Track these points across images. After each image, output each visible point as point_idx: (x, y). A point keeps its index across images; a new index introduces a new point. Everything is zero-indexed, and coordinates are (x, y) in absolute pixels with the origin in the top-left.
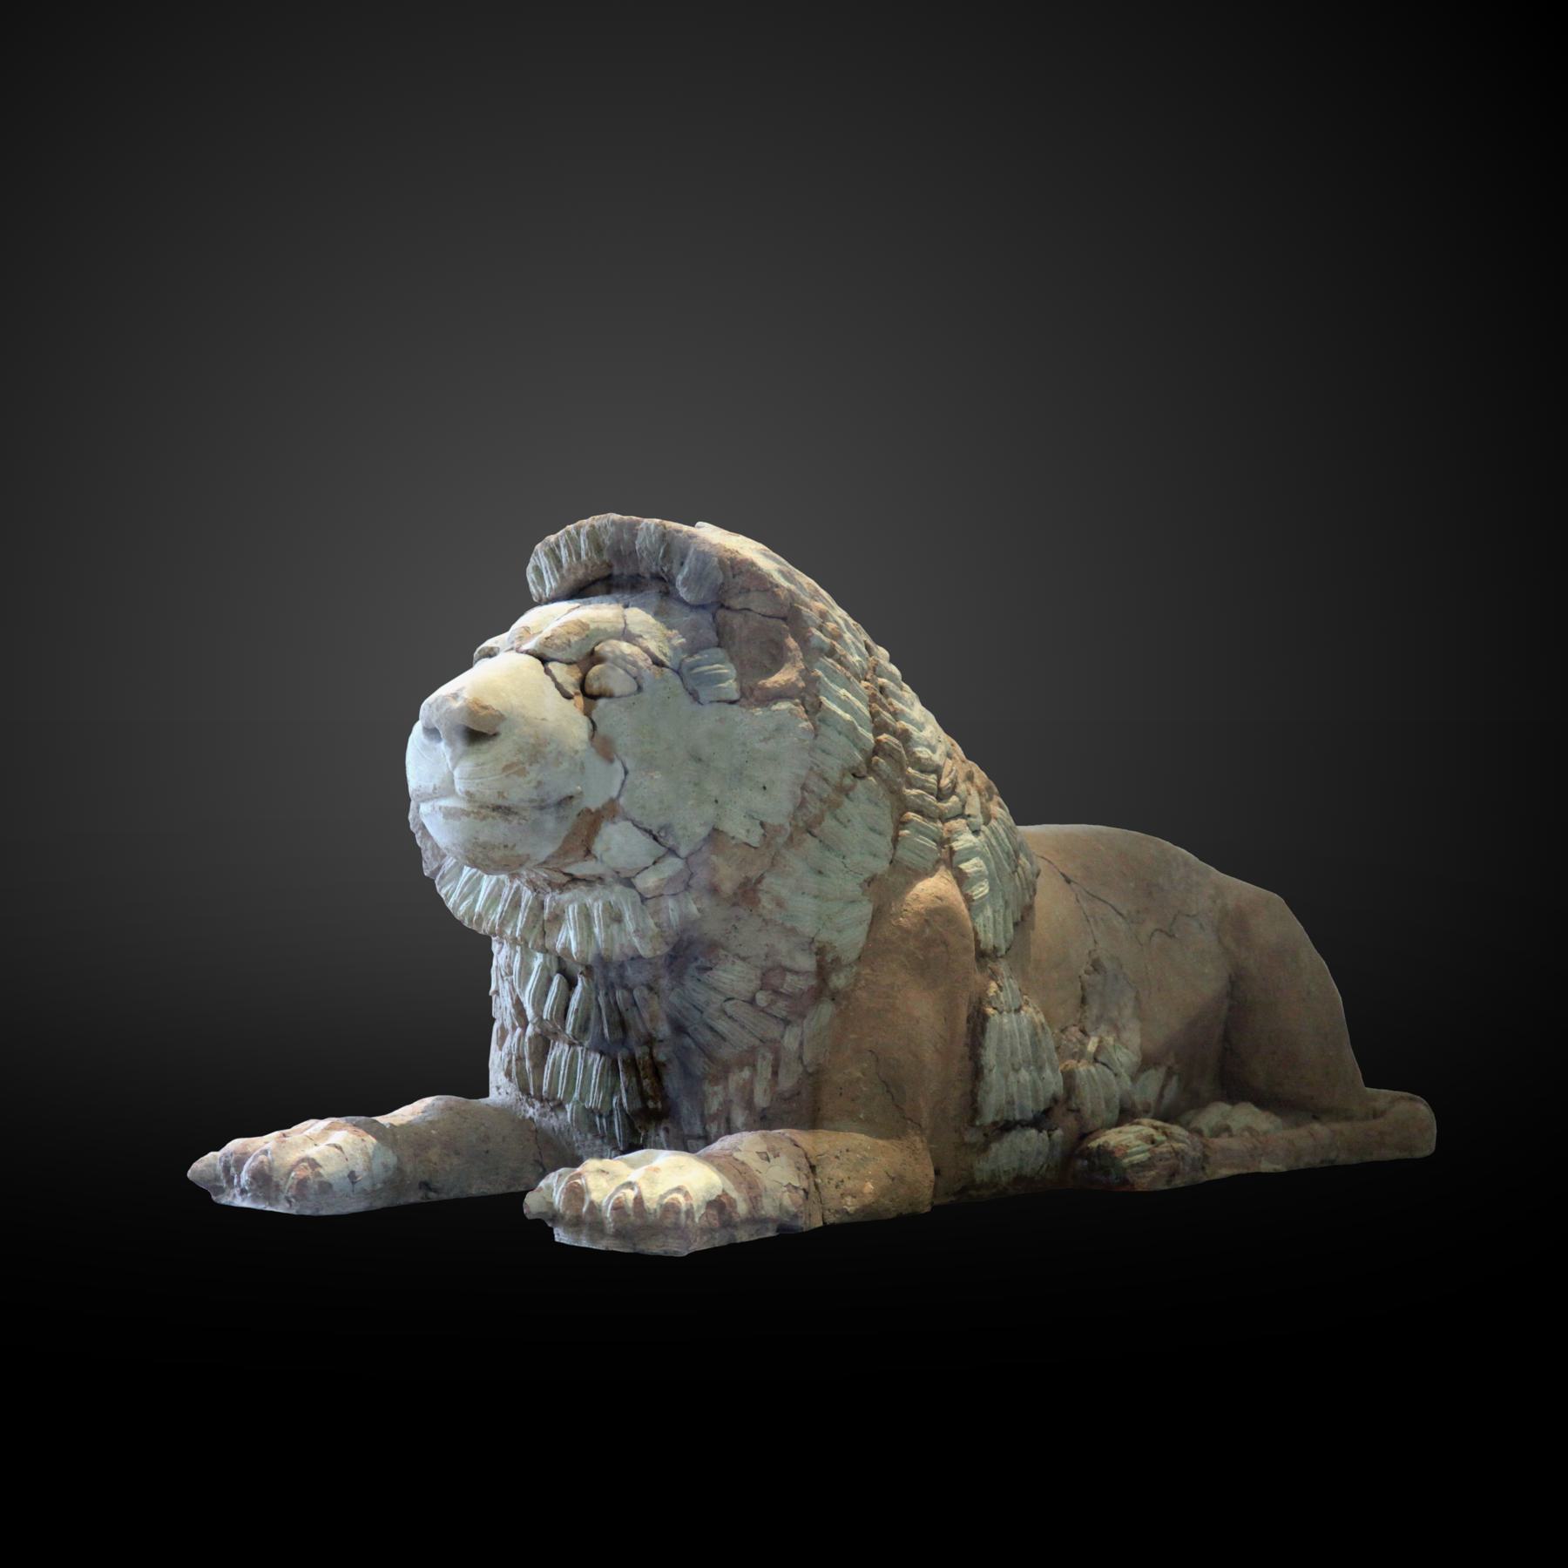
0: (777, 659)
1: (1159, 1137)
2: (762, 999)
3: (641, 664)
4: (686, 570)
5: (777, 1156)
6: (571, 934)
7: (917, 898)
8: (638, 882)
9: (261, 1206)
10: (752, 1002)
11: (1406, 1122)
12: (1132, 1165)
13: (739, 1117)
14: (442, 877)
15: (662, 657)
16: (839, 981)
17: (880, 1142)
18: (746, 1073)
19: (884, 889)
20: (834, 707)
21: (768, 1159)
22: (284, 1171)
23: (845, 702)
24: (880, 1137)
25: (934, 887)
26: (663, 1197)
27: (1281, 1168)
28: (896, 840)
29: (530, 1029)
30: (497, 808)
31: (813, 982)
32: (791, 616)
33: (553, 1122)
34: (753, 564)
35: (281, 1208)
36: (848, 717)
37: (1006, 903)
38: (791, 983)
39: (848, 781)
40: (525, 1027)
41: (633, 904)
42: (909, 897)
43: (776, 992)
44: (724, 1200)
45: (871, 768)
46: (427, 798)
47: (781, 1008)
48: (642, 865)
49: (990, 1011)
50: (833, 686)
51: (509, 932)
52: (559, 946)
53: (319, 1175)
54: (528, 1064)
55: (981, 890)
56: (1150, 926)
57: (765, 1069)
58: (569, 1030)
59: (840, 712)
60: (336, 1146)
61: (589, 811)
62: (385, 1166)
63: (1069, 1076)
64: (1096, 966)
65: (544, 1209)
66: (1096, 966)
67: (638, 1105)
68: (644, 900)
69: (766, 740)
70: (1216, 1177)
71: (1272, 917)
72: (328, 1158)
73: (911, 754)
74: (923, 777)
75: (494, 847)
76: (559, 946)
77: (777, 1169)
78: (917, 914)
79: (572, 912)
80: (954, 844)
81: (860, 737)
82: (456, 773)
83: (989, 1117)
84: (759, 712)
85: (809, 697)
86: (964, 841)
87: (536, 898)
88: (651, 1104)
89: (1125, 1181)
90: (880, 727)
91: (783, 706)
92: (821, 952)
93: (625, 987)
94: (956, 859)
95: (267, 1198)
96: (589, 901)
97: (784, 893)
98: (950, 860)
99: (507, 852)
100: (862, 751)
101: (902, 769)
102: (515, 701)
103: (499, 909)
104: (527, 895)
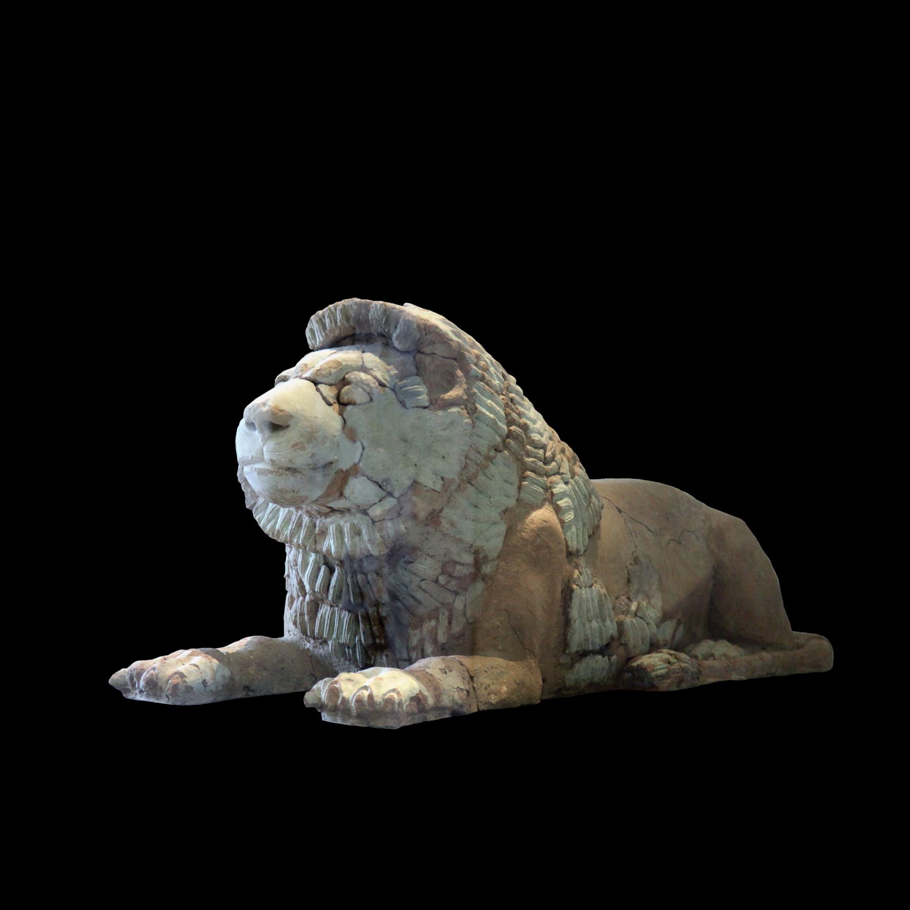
0: (451, 382)
1: (673, 660)
2: (442, 579)
3: (372, 385)
4: (398, 331)
5: (451, 671)
6: (332, 542)
7: (532, 521)
8: (370, 512)
9: (152, 700)
10: (436, 581)
11: (816, 651)
12: (657, 676)
13: (429, 648)
14: (257, 509)
15: (384, 382)
16: (487, 569)
17: (511, 663)
18: (433, 623)
19: (513, 516)
20: (484, 410)
21: (446, 673)
22: (165, 679)
23: (490, 408)
24: (511, 660)
25: (542, 515)
26: (385, 695)
27: (743, 678)
28: (520, 488)
29: (307, 597)
30: (288, 469)
31: (472, 570)
32: (459, 358)
33: (321, 651)
34: (437, 327)
35: (163, 701)
36: (492, 416)
37: (584, 524)
38: (459, 571)
39: (492, 453)
40: (304, 596)
41: (368, 525)
42: (528, 521)
43: (450, 576)
44: (420, 696)
45: (506, 446)
46: (248, 463)
47: (453, 585)
48: (373, 502)
49: (575, 587)
50: (483, 398)
51: (295, 541)
52: (324, 549)
53: (185, 682)
54: (306, 617)
55: (569, 517)
56: (668, 537)
57: (444, 620)
58: (330, 598)
59: (487, 413)
60: (195, 665)
61: (342, 470)
62: (224, 677)
63: (620, 625)
64: (636, 561)
65: (316, 702)
66: (636, 561)
67: (370, 641)
68: (374, 522)
69: (444, 429)
70: (706, 683)
71: (737, 531)
72: (190, 672)
73: (528, 437)
74: (536, 451)
75: (286, 492)
76: (324, 549)
77: (451, 678)
78: (532, 530)
79: (332, 529)
80: (554, 490)
81: (499, 428)
82: (265, 449)
83: (574, 648)
84: (440, 413)
85: (469, 405)
86: (560, 488)
87: (311, 521)
88: (378, 641)
89: (653, 686)
90: (511, 422)
91: (454, 410)
92: (476, 552)
93: (363, 573)
94: (555, 498)
95: (155, 695)
96: (342, 523)
97: (455, 518)
98: (551, 499)
99: (294, 495)
100: (500, 436)
101: (524, 447)
102: (299, 407)
103: (290, 528)
104: (306, 519)
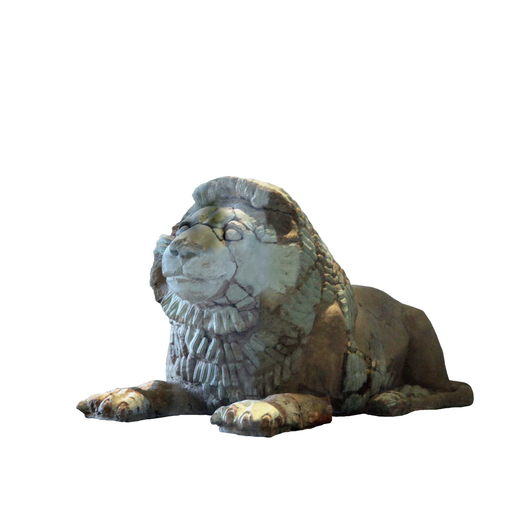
0: (289, 228)
1: (398, 397)
2: (279, 347)
3: (243, 229)
4: (255, 196)
5: (289, 403)
6: (214, 323)
7: (330, 312)
8: (238, 306)
10: (275, 348)
12: (391, 407)
13: (268, 389)
15: (249, 227)
16: (304, 341)
17: (318, 398)
18: (271, 373)
20: (306, 245)
21: (286, 404)
22: (116, 406)
25: (334, 308)
26: (262, 417)
28: (322, 292)
29: (189, 357)
30: (198, 279)
31: (296, 341)
33: (196, 390)
34: (280, 195)
37: (352, 314)
38: (290, 342)
39: (310, 271)
40: (186, 356)
41: (235, 313)
42: (327, 312)
43: (283, 345)
45: (316, 267)
46: (170, 275)
47: (285, 351)
48: (239, 300)
50: (306, 238)
51: (190, 322)
52: (209, 328)
53: (128, 408)
54: (187, 369)
55: (346, 310)
56: (384, 322)
57: (278, 371)
58: (207, 357)
59: (308, 247)
60: (132, 398)
62: (147, 405)
64: (372, 335)
66: (372, 335)
67: (229, 384)
68: (239, 312)
69: (287, 256)
72: (131, 402)
73: (326, 261)
74: (329, 269)
75: (196, 293)
76: (209, 328)
77: (290, 407)
78: (330, 318)
79: (214, 316)
80: (339, 293)
81: (313, 255)
82: (184, 267)
83: (346, 390)
84: (284, 246)
85: (298, 240)
86: (341, 292)
87: (201, 311)
88: (233, 384)
90: (318, 252)
91: (293, 245)
92: (300, 331)
93: (227, 342)
94: (339, 298)
96: (221, 312)
97: (289, 310)
98: (338, 299)
99: (201, 295)
100: (314, 260)
101: (323, 267)
103: (186, 314)
104: (197, 310)
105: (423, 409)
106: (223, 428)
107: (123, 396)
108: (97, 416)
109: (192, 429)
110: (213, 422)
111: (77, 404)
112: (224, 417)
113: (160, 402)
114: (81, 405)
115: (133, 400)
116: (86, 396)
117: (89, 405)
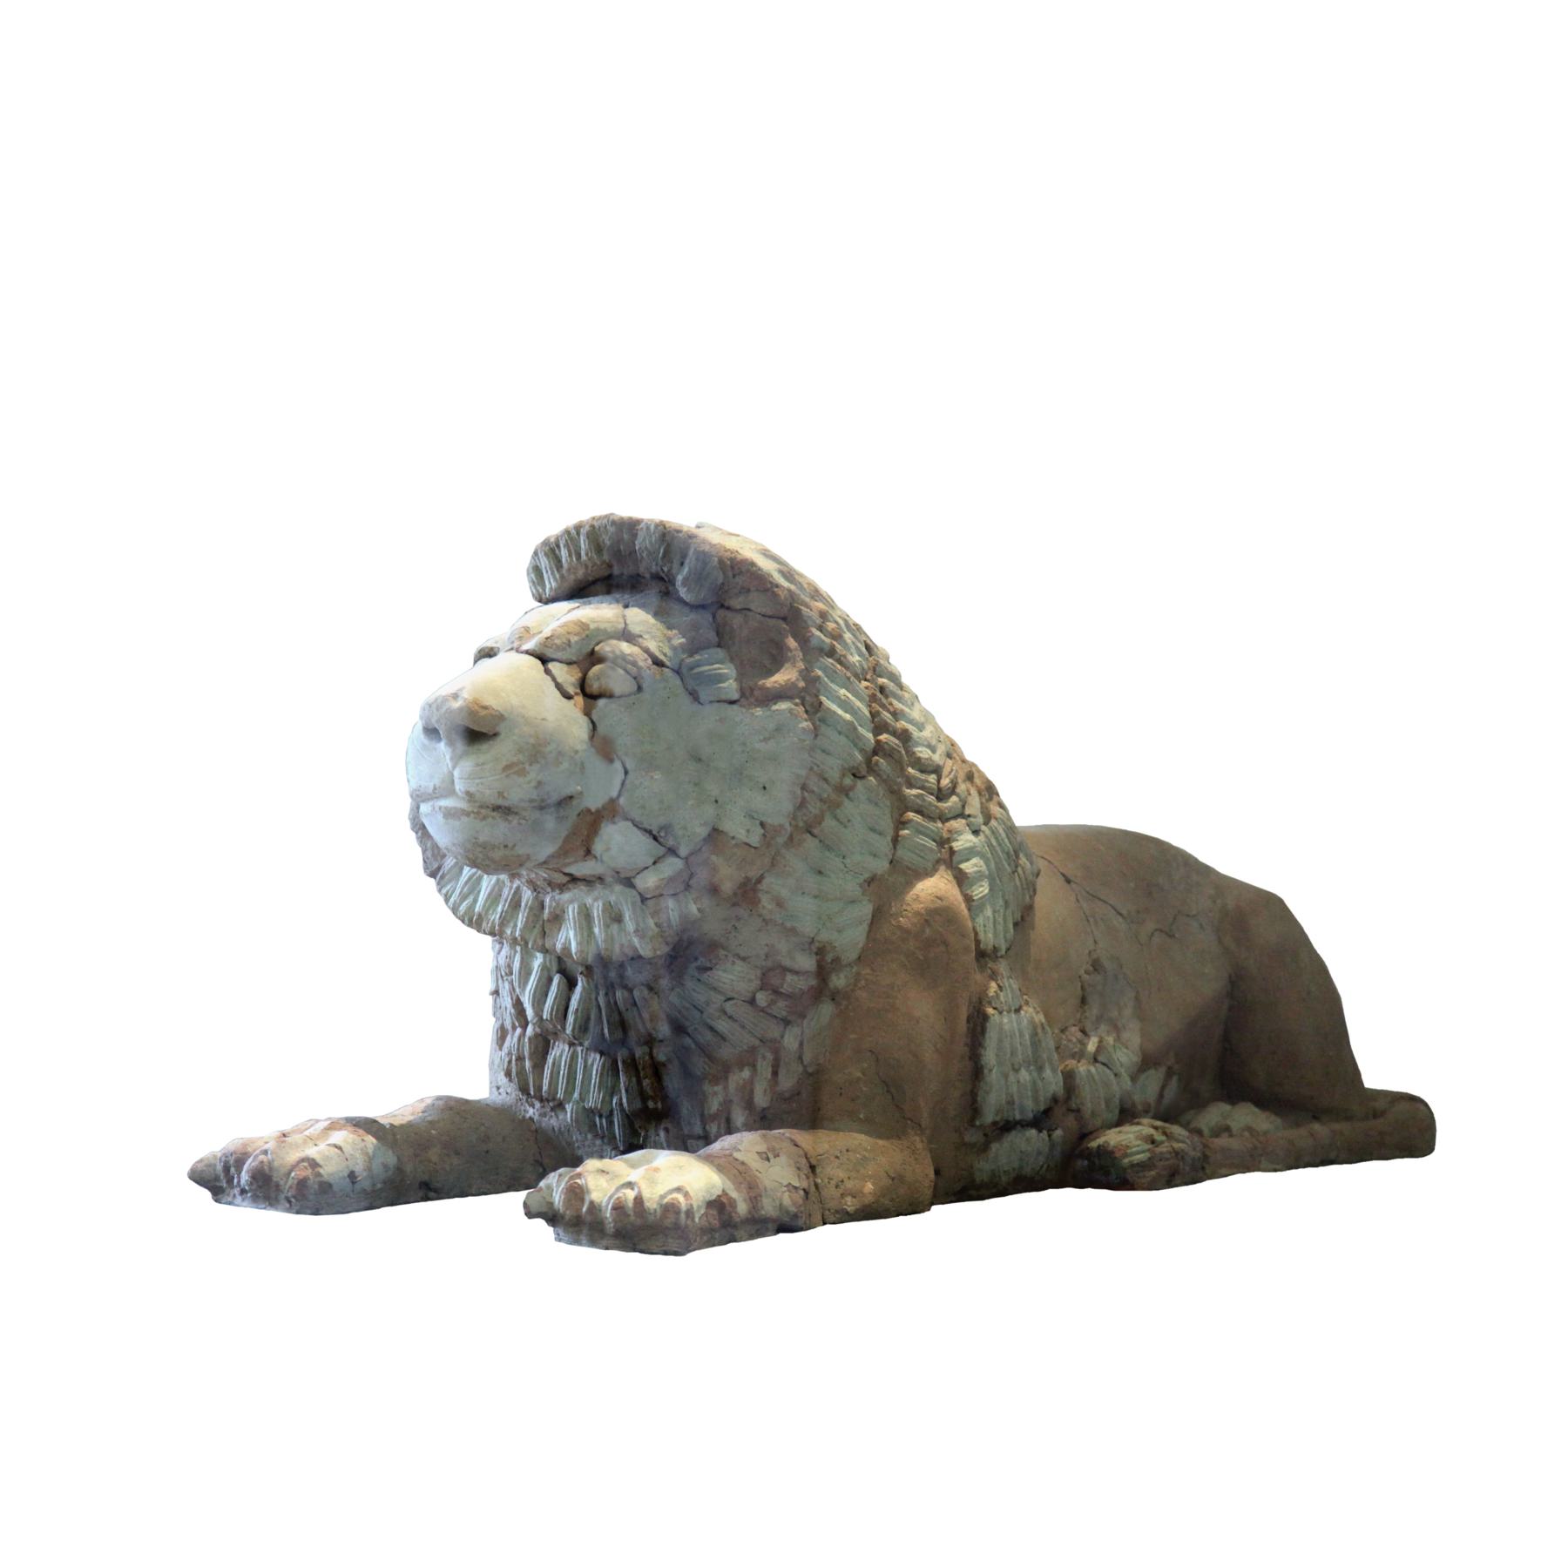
0: (777, 659)
1: (1159, 1137)
2: (762, 999)
3: (641, 664)
4: (686, 570)
5: (777, 1156)
6: (571, 934)
7: (917, 898)
8: (638, 882)
10: (752, 1002)
12: (1132, 1165)
13: (739, 1117)
15: (662, 657)
16: (839, 981)
17: (880, 1142)
18: (746, 1073)
19: (884, 889)
20: (834, 707)
21: (768, 1159)
22: (284, 1171)
24: (880, 1137)
25: (934, 887)
28: (896, 840)
29: (530, 1029)
30: (497, 808)
31: (813, 982)
33: (553, 1122)
34: (753, 564)
36: (848, 717)
37: (1006, 903)
38: (791, 983)
39: (848, 781)
40: (525, 1027)
41: (633, 904)
42: (909, 897)
43: (776, 992)
44: (724, 1200)
45: (871, 768)
47: (781, 1008)
48: (642, 865)
49: (990, 1011)
50: (833, 686)
51: (509, 932)
52: (559, 946)
53: (319, 1175)
54: (528, 1064)
55: (981, 890)
56: (1150, 926)
57: (765, 1069)
58: (569, 1030)
59: (840, 712)
60: (336, 1146)
61: (589, 811)
62: (385, 1166)
63: (1069, 1076)
64: (1096, 966)
66: (1096, 966)
67: (638, 1105)
68: (644, 900)
69: (766, 740)
72: (328, 1158)
73: (911, 754)
74: (923, 777)
76: (559, 946)
77: (777, 1169)
78: (917, 914)
79: (572, 912)
80: (954, 844)
81: (860, 737)
82: (456, 773)
83: (989, 1117)
84: (759, 712)
85: (809, 697)
86: (964, 841)
87: (536, 898)
88: (651, 1104)
90: (880, 727)
91: (783, 706)
92: (821, 952)
93: (625, 987)
94: (956, 859)
96: (589, 901)
97: (784, 893)
98: (950, 860)
99: (507, 852)
100: (862, 751)
101: (902, 769)
102: (515, 701)
103: (499, 909)
104: (527, 895)
105: (463, 1194)
106: (560, 1231)
107: (314, 1140)
108: (239, 1199)
109: (491, 1227)
110: (530, 1214)
111: (188, 1168)
112: (558, 1199)
113: (429, 1161)
114: (200, 1166)
115: (339, 1153)
116: (212, 1144)
117: (219, 1167)
